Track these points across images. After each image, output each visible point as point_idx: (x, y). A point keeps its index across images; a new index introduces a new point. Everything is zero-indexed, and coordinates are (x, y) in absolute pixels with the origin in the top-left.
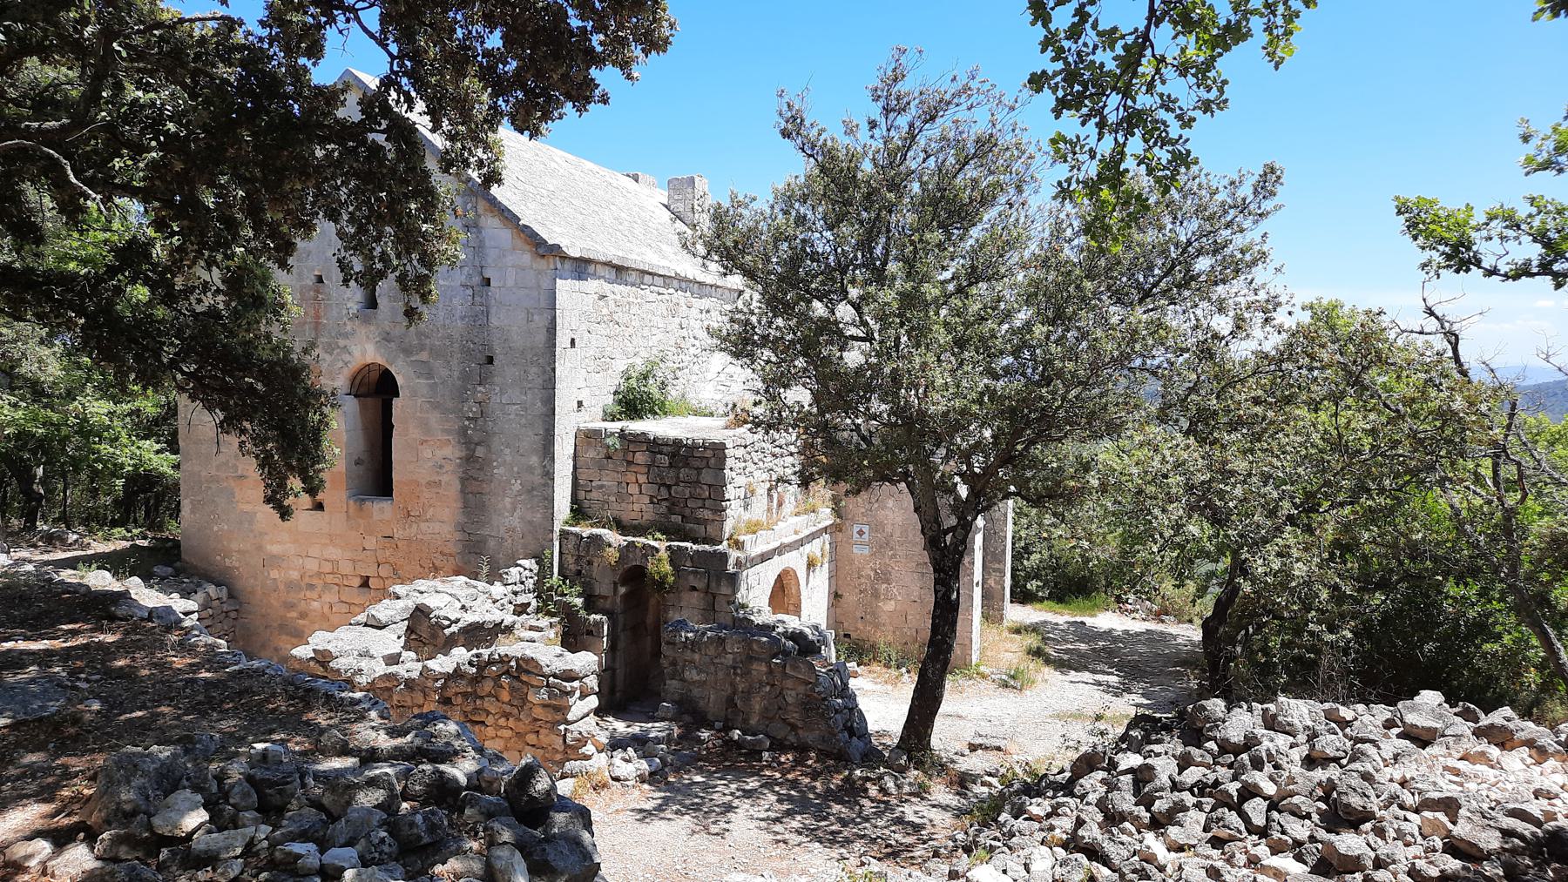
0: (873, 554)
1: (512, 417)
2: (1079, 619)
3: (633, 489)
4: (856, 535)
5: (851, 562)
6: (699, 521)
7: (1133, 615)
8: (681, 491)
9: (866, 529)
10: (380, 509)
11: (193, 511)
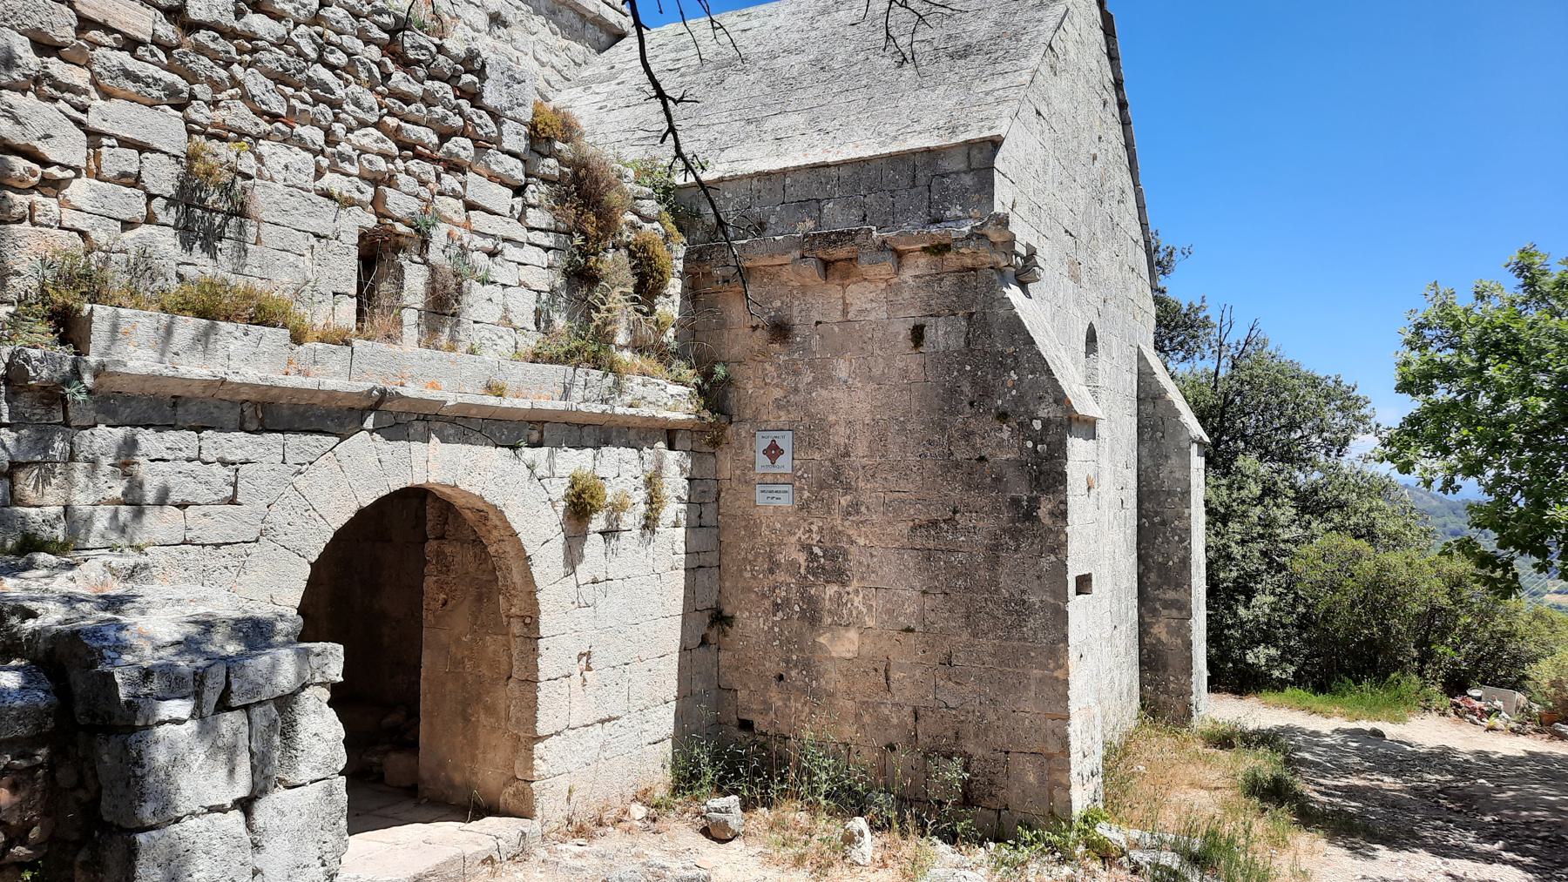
0: (804, 506)
2: (1366, 725)
4: (762, 461)
5: (752, 528)
7: (1487, 722)
9: (785, 442)
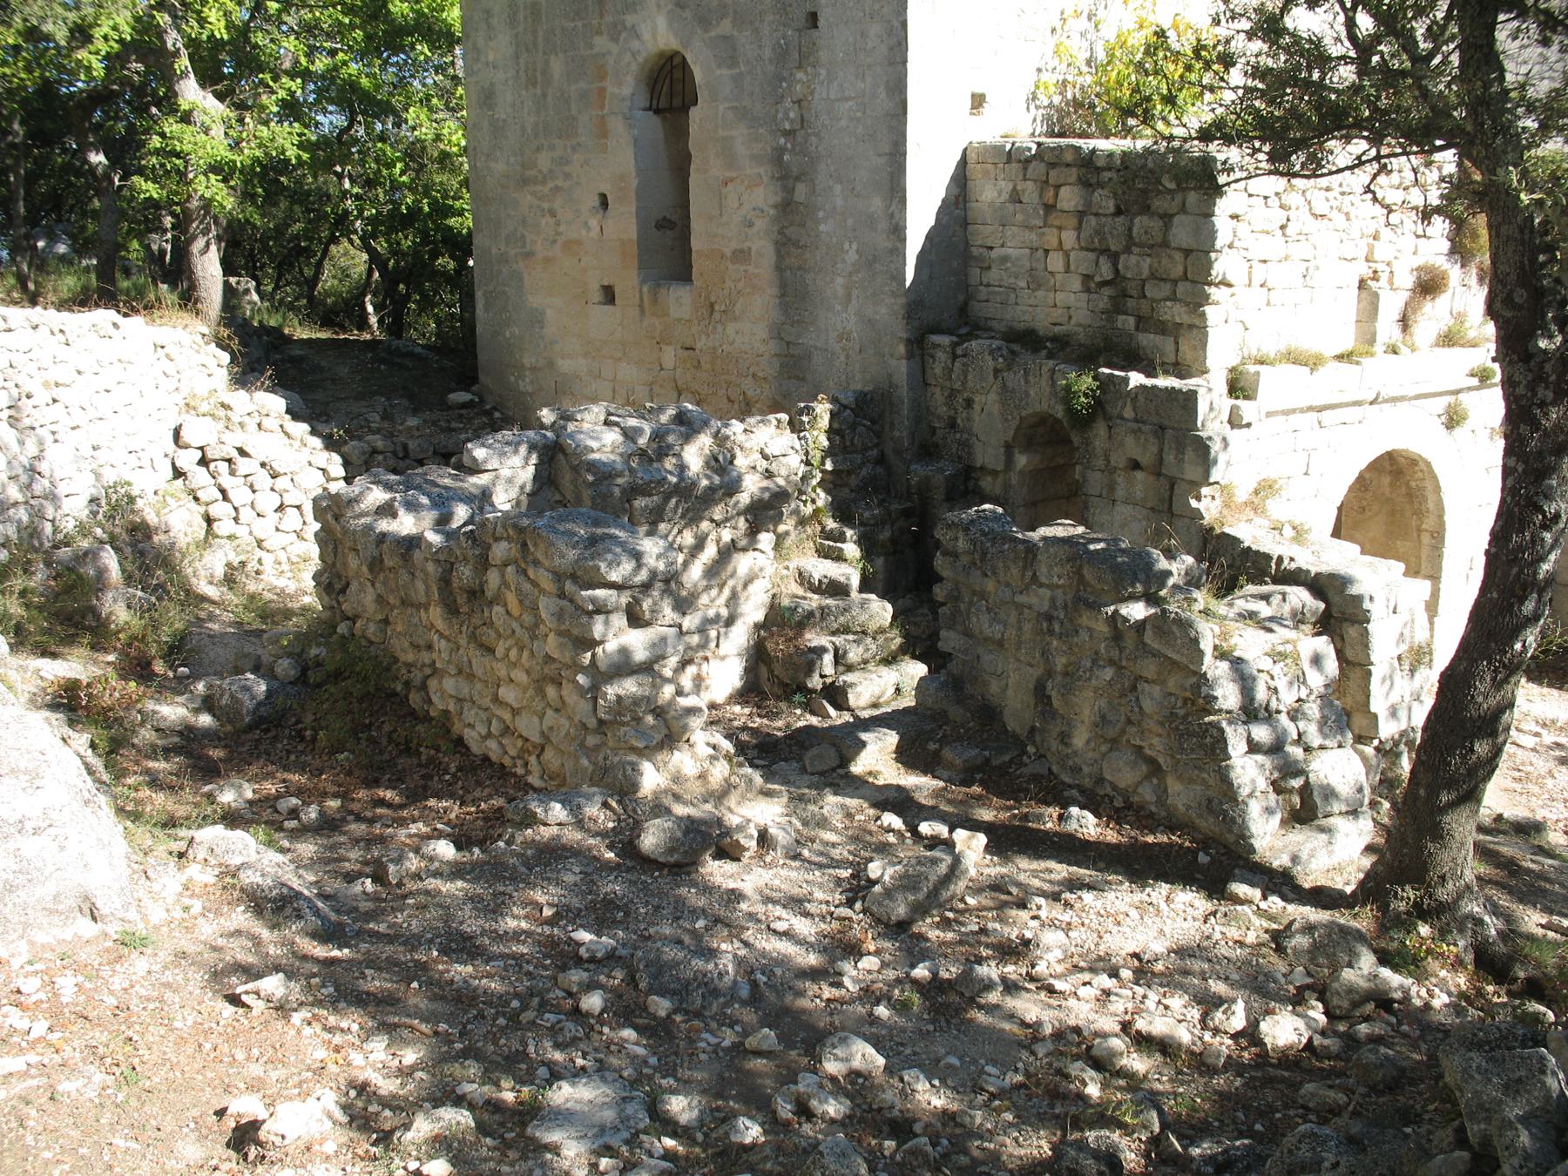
1: (844, 123)
3: (1056, 262)
6: (1163, 329)
8: (1136, 264)
10: (679, 300)
11: (486, 310)
